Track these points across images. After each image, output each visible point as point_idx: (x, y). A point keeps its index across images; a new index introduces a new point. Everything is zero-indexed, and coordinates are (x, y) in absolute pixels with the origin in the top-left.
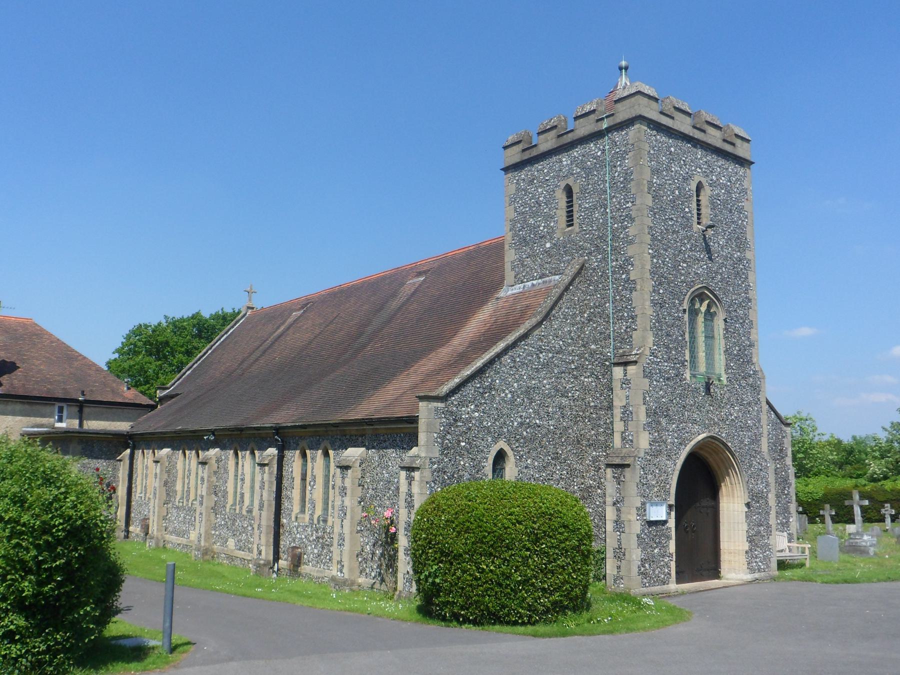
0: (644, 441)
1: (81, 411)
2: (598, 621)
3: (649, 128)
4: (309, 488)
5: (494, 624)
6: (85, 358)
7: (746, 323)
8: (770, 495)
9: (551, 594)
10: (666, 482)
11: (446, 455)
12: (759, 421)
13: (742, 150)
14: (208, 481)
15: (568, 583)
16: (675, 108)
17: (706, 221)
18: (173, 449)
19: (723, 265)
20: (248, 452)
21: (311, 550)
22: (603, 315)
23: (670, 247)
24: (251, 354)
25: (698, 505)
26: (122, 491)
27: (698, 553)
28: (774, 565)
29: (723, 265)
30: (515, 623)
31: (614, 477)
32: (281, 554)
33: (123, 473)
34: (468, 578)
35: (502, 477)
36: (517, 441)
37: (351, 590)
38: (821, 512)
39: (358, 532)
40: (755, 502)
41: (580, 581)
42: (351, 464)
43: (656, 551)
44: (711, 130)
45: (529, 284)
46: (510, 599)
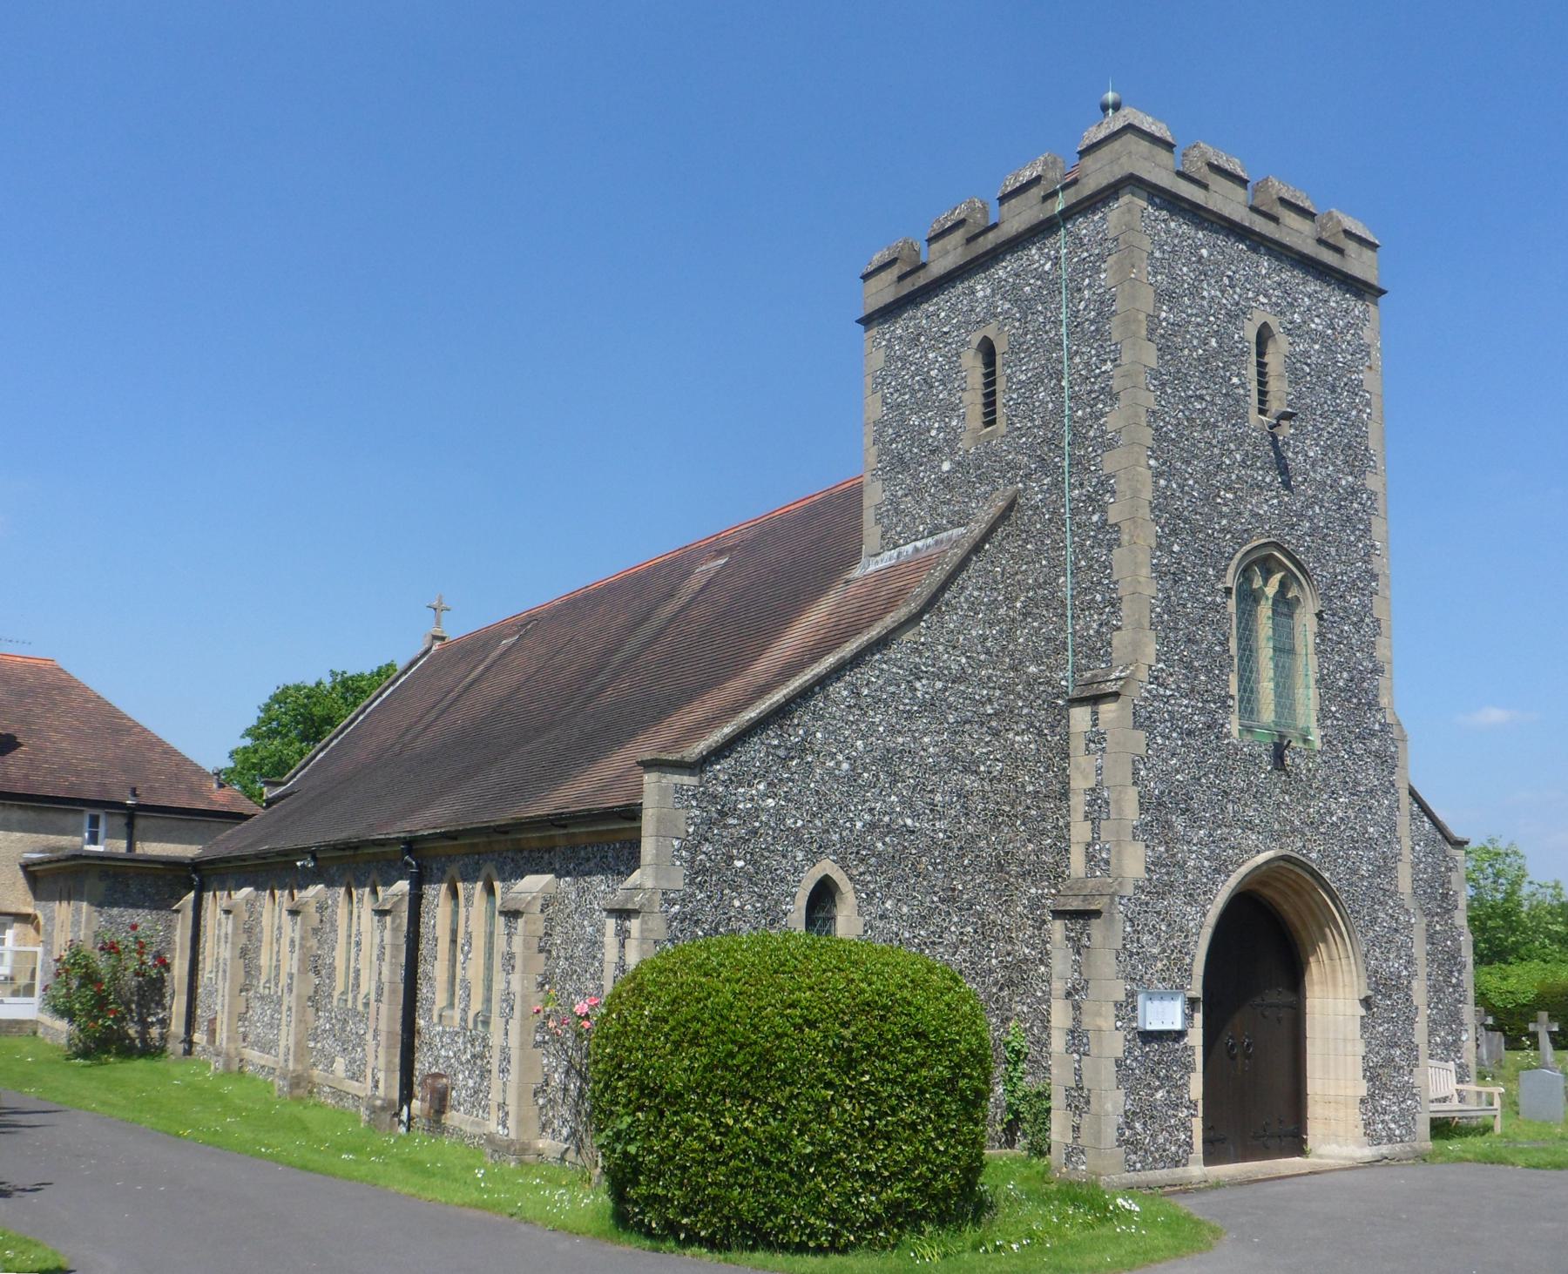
0: (1133, 863)
1: (130, 825)
2: (997, 1249)
3: (1152, 204)
4: (460, 958)
5: (753, 1249)
6: (145, 730)
7: (1367, 624)
8: (1415, 984)
9: (884, 1187)
10: (1183, 950)
11: (701, 886)
12: (1393, 829)
13: (1359, 264)
14: (302, 946)
15: (925, 1161)
16: (1210, 165)
17: (1276, 406)
18: (257, 889)
19: (1315, 500)
20: (367, 890)
21: (464, 1081)
22: (1054, 603)
23: (1196, 457)
24: (421, 717)
25: (1258, 1000)
26: (180, 968)
27: (1255, 1099)
28: (1424, 1128)
29: (1315, 500)
30: (801, 1248)
31: (1068, 938)
32: (417, 1089)
33: (182, 935)
34: (696, 1145)
35: (828, 932)
36: (862, 860)
37: (521, 1162)
38: (1531, 1027)
39: (537, 1045)
40: (1382, 998)
41: (955, 1157)
42: (521, 907)
43: (1159, 1095)
44: (1290, 218)
45: (909, 548)
46: (789, 1194)
